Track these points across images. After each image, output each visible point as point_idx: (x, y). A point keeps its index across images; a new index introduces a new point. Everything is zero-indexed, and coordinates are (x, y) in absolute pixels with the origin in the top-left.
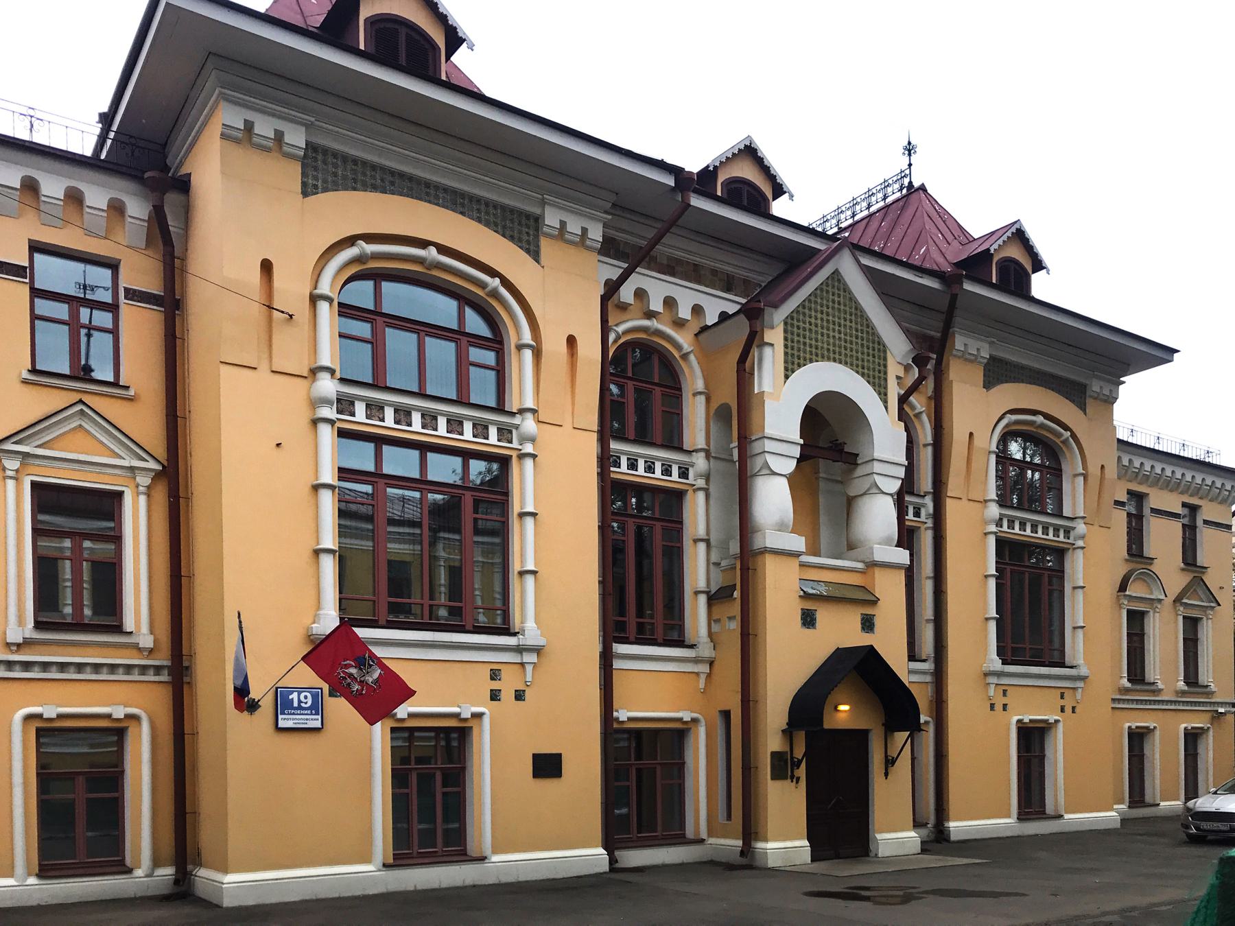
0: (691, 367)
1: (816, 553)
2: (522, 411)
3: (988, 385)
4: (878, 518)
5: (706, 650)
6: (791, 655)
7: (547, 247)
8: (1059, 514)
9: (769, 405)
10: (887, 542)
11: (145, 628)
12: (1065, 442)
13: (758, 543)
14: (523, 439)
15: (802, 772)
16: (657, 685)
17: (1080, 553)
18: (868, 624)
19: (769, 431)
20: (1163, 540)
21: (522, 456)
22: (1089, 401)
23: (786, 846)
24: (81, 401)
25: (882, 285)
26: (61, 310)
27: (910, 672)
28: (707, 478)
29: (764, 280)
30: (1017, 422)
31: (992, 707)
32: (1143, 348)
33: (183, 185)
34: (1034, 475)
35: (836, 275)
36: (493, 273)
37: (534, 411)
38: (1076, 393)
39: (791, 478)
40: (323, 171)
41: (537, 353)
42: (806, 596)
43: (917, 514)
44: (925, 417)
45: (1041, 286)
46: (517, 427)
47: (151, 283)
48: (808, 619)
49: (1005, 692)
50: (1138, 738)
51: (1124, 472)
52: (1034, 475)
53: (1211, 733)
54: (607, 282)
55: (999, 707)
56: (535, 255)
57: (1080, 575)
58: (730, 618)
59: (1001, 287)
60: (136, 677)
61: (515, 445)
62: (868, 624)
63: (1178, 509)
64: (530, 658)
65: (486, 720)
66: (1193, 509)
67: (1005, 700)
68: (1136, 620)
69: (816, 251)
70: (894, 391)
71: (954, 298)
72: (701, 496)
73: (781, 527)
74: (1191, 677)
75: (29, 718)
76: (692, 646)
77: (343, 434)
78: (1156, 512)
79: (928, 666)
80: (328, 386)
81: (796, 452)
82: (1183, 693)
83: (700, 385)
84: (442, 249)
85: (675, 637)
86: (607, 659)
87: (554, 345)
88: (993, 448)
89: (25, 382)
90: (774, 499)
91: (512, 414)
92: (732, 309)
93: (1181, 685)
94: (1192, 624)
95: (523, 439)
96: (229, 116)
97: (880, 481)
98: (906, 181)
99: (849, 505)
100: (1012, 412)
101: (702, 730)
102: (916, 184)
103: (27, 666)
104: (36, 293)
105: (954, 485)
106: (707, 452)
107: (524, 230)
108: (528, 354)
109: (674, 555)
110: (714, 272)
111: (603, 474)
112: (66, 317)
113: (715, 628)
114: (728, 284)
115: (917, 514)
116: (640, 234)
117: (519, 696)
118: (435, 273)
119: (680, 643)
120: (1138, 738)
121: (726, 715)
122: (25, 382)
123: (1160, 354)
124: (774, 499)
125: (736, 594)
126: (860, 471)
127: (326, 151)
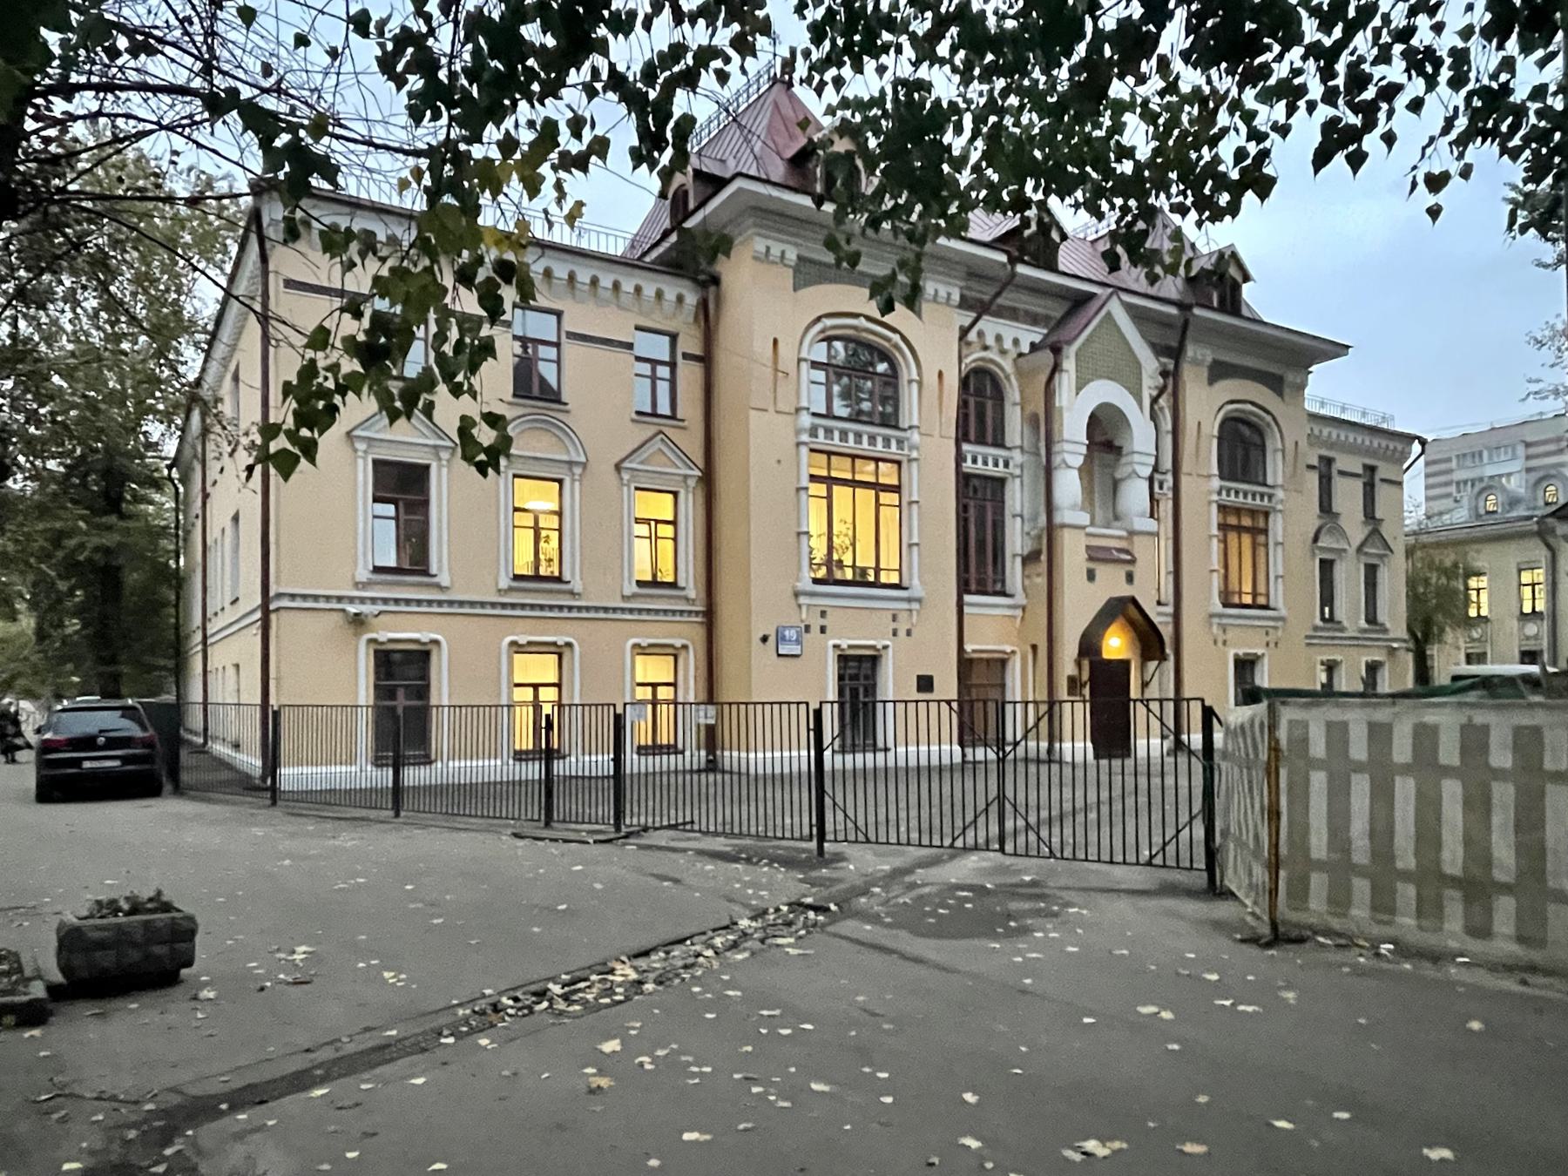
1: (1092, 524)
2: (911, 427)
3: (1212, 380)
4: (1135, 495)
5: (1020, 599)
6: (1081, 602)
9: (1066, 415)
11: (691, 584)
13: (1058, 519)
14: (911, 448)
15: (1087, 691)
16: (993, 626)
18: (1130, 578)
19: (1066, 436)
20: (1348, 496)
21: (910, 461)
23: (1077, 746)
25: (1137, 314)
27: (1159, 614)
28: (1022, 467)
29: (1058, 314)
31: (1215, 642)
32: (1323, 346)
33: (716, 280)
34: (1242, 447)
35: (1109, 314)
38: (1275, 383)
39: (1080, 469)
40: (806, 274)
41: (920, 383)
42: (1091, 559)
43: (1161, 487)
44: (1013, 378)
47: (697, 350)
48: (1091, 576)
49: (823, 614)
51: (1313, 440)
52: (1242, 447)
53: (1387, 666)
54: (961, 327)
55: (1220, 644)
57: (1280, 533)
58: (1039, 575)
59: (1222, 309)
60: (678, 618)
61: (906, 452)
62: (1130, 578)
63: (1360, 471)
64: (915, 606)
65: (890, 650)
66: (1371, 469)
68: (1327, 567)
69: (1092, 296)
70: (1147, 402)
71: (1186, 324)
72: (1018, 481)
73: (1073, 507)
74: (1372, 619)
75: (836, 647)
77: (812, 450)
78: (1342, 473)
79: (1170, 609)
80: (806, 420)
81: (1084, 450)
82: (1365, 631)
83: (1017, 398)
85: (998, 587)
86: (960, 605)
87: (931, 379)
88: (1216, 432)
90: (1069, 486)
92: (1037, 339)
93: (1363, 623)
94: (1371, 571)
96: (760, 245)
97: (1138, 468)
99: (1115, 485)
100: (1232, 402)
103: (631, 611)
105: (1186, 467)
106: (1021, 448)
108: (915, 386)
109: (999, 526)
111: (958, 465)
113: (1027, 582)
114: (1034, 320)
116: (986, 292)
117: (909, 633)
118: (864, 335)
119: (1003, 594)
121: (1034, 648)
122: (633, 421)
123: (1340, 350)
124: (1069, 486)
125: (1044, 557)
126: (1124, 460)
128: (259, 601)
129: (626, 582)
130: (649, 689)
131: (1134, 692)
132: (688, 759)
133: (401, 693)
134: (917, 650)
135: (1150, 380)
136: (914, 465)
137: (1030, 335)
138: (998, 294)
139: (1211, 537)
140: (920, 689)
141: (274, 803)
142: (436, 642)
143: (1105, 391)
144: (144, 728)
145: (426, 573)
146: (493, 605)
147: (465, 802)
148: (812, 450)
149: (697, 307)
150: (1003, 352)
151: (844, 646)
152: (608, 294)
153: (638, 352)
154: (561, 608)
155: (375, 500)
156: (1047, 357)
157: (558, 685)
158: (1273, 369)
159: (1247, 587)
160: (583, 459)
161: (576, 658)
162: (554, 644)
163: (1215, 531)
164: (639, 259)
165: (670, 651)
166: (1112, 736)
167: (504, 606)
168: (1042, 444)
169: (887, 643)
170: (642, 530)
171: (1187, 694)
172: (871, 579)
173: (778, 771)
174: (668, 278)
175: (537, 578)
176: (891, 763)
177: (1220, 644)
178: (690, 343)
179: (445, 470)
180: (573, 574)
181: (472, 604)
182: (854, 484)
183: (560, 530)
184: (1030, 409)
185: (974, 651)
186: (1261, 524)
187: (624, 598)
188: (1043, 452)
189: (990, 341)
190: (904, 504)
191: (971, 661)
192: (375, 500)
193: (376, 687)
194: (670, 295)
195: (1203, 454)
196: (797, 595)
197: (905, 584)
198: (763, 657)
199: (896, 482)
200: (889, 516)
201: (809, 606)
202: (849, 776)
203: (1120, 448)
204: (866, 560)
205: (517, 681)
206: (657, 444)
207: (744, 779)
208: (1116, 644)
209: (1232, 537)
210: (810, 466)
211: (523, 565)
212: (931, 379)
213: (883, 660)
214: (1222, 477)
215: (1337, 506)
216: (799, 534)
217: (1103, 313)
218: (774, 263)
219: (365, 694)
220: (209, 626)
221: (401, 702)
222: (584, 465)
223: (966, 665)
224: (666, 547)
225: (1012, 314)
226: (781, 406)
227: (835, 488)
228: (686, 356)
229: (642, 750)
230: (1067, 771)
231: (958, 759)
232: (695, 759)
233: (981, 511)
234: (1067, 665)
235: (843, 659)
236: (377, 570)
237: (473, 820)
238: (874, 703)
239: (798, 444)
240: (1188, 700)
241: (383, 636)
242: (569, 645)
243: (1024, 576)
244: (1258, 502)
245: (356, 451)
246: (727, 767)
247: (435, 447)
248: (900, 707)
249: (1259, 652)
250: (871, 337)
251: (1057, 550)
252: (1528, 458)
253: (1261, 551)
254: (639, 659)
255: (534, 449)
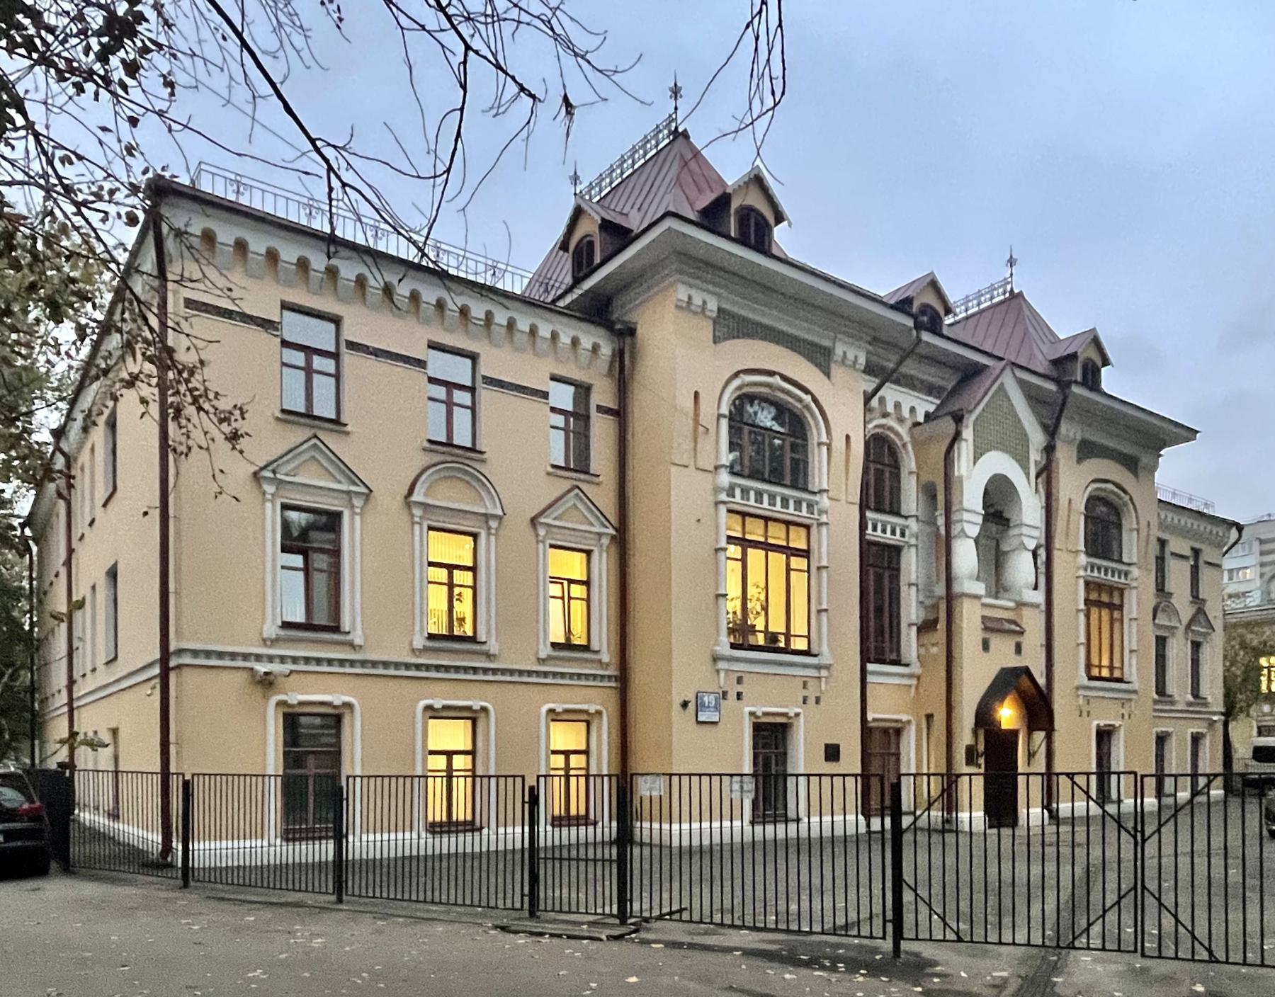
0: (907, 453)
2: (821, 491)
4: (1022, 569)
5: (916, 669)
7: (836, 370)
8: (1120, 561)
9: (966, 485)
10: (970, 578)
12: (1125, 504)
13: (957, 589)
14: (821, 512)
16: (891, 696)
17: (1134, 592)
19: (966, 505)
20: (1178, 575)
21: (820, 525)
22: (1139, 471)
23: (973, 816)
24: (316, 436)
26: (299, 358)
30: (1097, 489)
33: (632, 332)
35: (1002, 384)
36: (807, 391)
37: (827, 491)
38: (1131, 464)
39: (976, 541)
40: (730, 327)
41: (829, 447)
42: (986, 629)
44: (910, 447)
45: (1109, 380)
46: (817, 503)
48: (986, 646)
49: (740, 681)
50: (1161, 740)
53: (1208, 737)
55: (1085, 714)
56: (828, 374)
64: (824, 673)
65: (802, 716)
66: (1196, 552)
67: (740, 688)
68: (1161, 642)
74: (1196, 693)
75: (752, 714)
76: (907, 665)
77: (730, 511)
81: (980, 520)
82: (1190, 704)
83: (913, 466)
84: (785, 378)
85: (894, 657)
87: (839, 443)
89: (424, 449)
90: (966, 557)
91: (814, 493)
92: (931, 408)
93: (1190, 698)
94: (1196, 646)
95: (821, 512)
96: (682, 293)
97: (1027, 541)
98: (1009, 287)
101: (913, 728)
102: (1016, 291)
103: (546, 674)
104: (285, 343)
105: (1058, 542)
107: (821, 358)
108: (824, 449)
110: (922, 382)
112: (302, 364)
113: (922, 651)
114: (930, 390)
115: (875, 529)
117: (818, 700)
119: (897, 663)
120: (1161, 740)
121: (929, 717)
122: (549, 474)
123: (1191, 434)
124: (966, 557)
125: (942, 626)
126: (1013, 532)
127: (733, 316)
128: (158, 656)
129: (541, 647)
130: (562, 757)
131: (1022, 766)
132: (599, 831)
133: (311, 761)
134: (824, 723)
135: (1035, 456)
136: (824, 529)
137: (925, 405)
138: (900, 363)
139: (1078, 611)
140: (827, 759)
141: (186, 885)
142: (348, 706)
143: (998, 463)
144: (29, 799)
145: (336, 629)
146: (408, 666)
147: (401, 885)
148: (730, 511)
149: (613, 355)
150: (901, 420)
151: (759, 714)
152: (525, 338)
153: (553, 402)
154: (475, 670)
155: (283, 551)
156: (948, 425)
157: (472, 753)
158: (1127, 449)
159: (1105, 662)
160: (500, 513)
161: (491, 727)
162: (469, 708)
163: (1082, 606)
164: (554, 301)
165: (585, 717)
166: (1001, 808)
167: (418, 667)
168: (940, 512)
169: (798, 710)
170: (555, 590)
171: (1058, 768)
172: (782, 645)
173: (685, 843)
174: (584, 325)
175: (451, 637)
176: (804, 834)
177: (1085, 714)
178: (603, 395)
179: (358, 518)
180: (489, 632)
181: (386, 664)
182: (767, 547)
183: (474, 588)
184: (925, 478)
185: (875, 720)
186: (1116, 601)
187: (541, 661)
188: (941, 521)
189: (890, 408)
190: (813, 570)
191: (871, 729)
192: (283, 551)
193: (285, 753)
194: (586, 343)
195: (1072, 531)
196: (716, 659)
197: (814, 651)
198: (681, 722)
199: (804, 547)
200: (799, 581)
201: (727, 671)
202: (770, 849)
203: (1008, 520)
204: (777, 626)
205: (431, 747)
206: (571, 500)
207: (666, 852)
208: (1008, 715)
209: (1094, 612)
210: (728, 529)
211: (437, 625)
212: (839, 443)
213: (795, 728)
214: (1088, 554)
215: (1171, 586)
216: (718, 596)
217: (998, 382)
218: (695, 313)
219: (273, 761)
220: (75, 688)
221: (312, 768)
222: (500, 518)
223: (867, 731)
224: (578, 608)
225: (910, 383)
226: (700, 464)
227: (750, 551)
228: (600, 409)
229: (557, 822)
230: (964, 840)
231: (862, 829)
232: (607, 830)
233: (879, 578)
234: (965, 737)
235: (758, 728)
236: (287, 625)
237: (414, 906)
238: (785, 776)
239: (717, 503)
240: (1058, 774)
241: (294, 698)
242: (484, 709)
243: (920, 645)
244: (1116, 579)
245: (264, 493)
246: (646, 839)
247: (349, 493)
248: (401, 780)
249: (1117, 723)
250: (782, 395)
251: (956, 620)
252: (1262, 553)
253: (1117, 625)
254: (552, 724)
255: (449, 499)
